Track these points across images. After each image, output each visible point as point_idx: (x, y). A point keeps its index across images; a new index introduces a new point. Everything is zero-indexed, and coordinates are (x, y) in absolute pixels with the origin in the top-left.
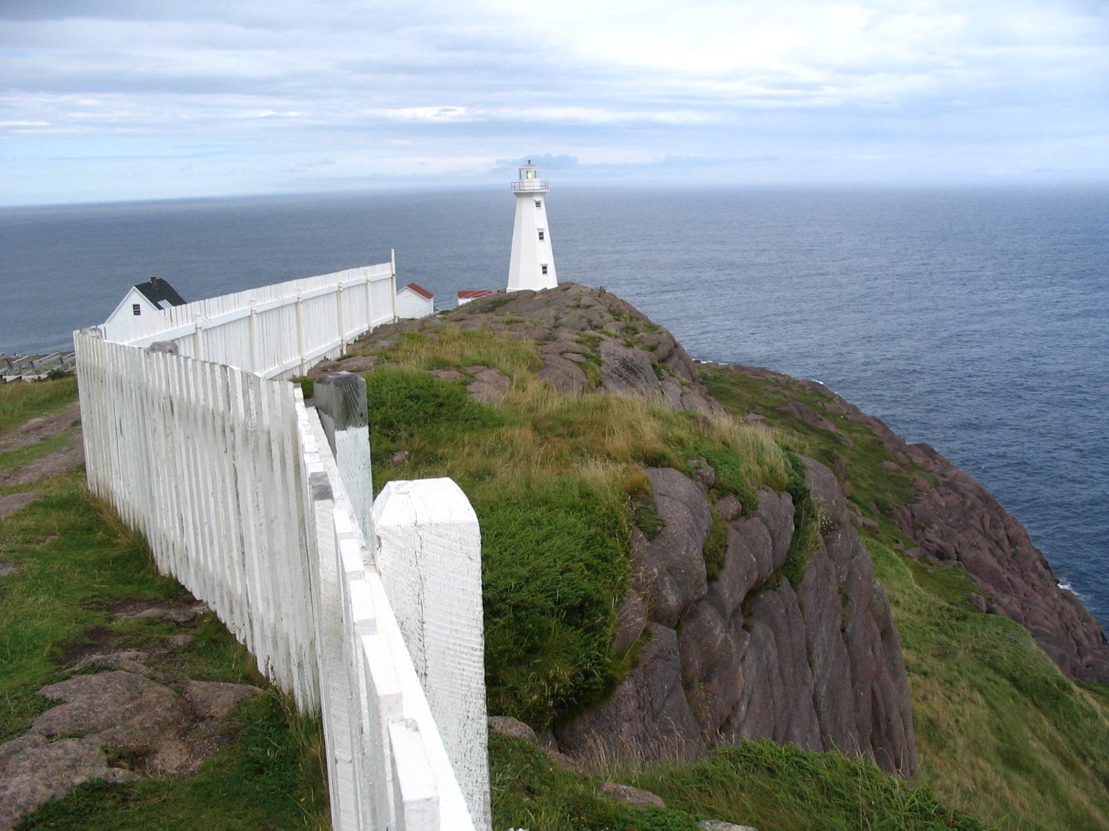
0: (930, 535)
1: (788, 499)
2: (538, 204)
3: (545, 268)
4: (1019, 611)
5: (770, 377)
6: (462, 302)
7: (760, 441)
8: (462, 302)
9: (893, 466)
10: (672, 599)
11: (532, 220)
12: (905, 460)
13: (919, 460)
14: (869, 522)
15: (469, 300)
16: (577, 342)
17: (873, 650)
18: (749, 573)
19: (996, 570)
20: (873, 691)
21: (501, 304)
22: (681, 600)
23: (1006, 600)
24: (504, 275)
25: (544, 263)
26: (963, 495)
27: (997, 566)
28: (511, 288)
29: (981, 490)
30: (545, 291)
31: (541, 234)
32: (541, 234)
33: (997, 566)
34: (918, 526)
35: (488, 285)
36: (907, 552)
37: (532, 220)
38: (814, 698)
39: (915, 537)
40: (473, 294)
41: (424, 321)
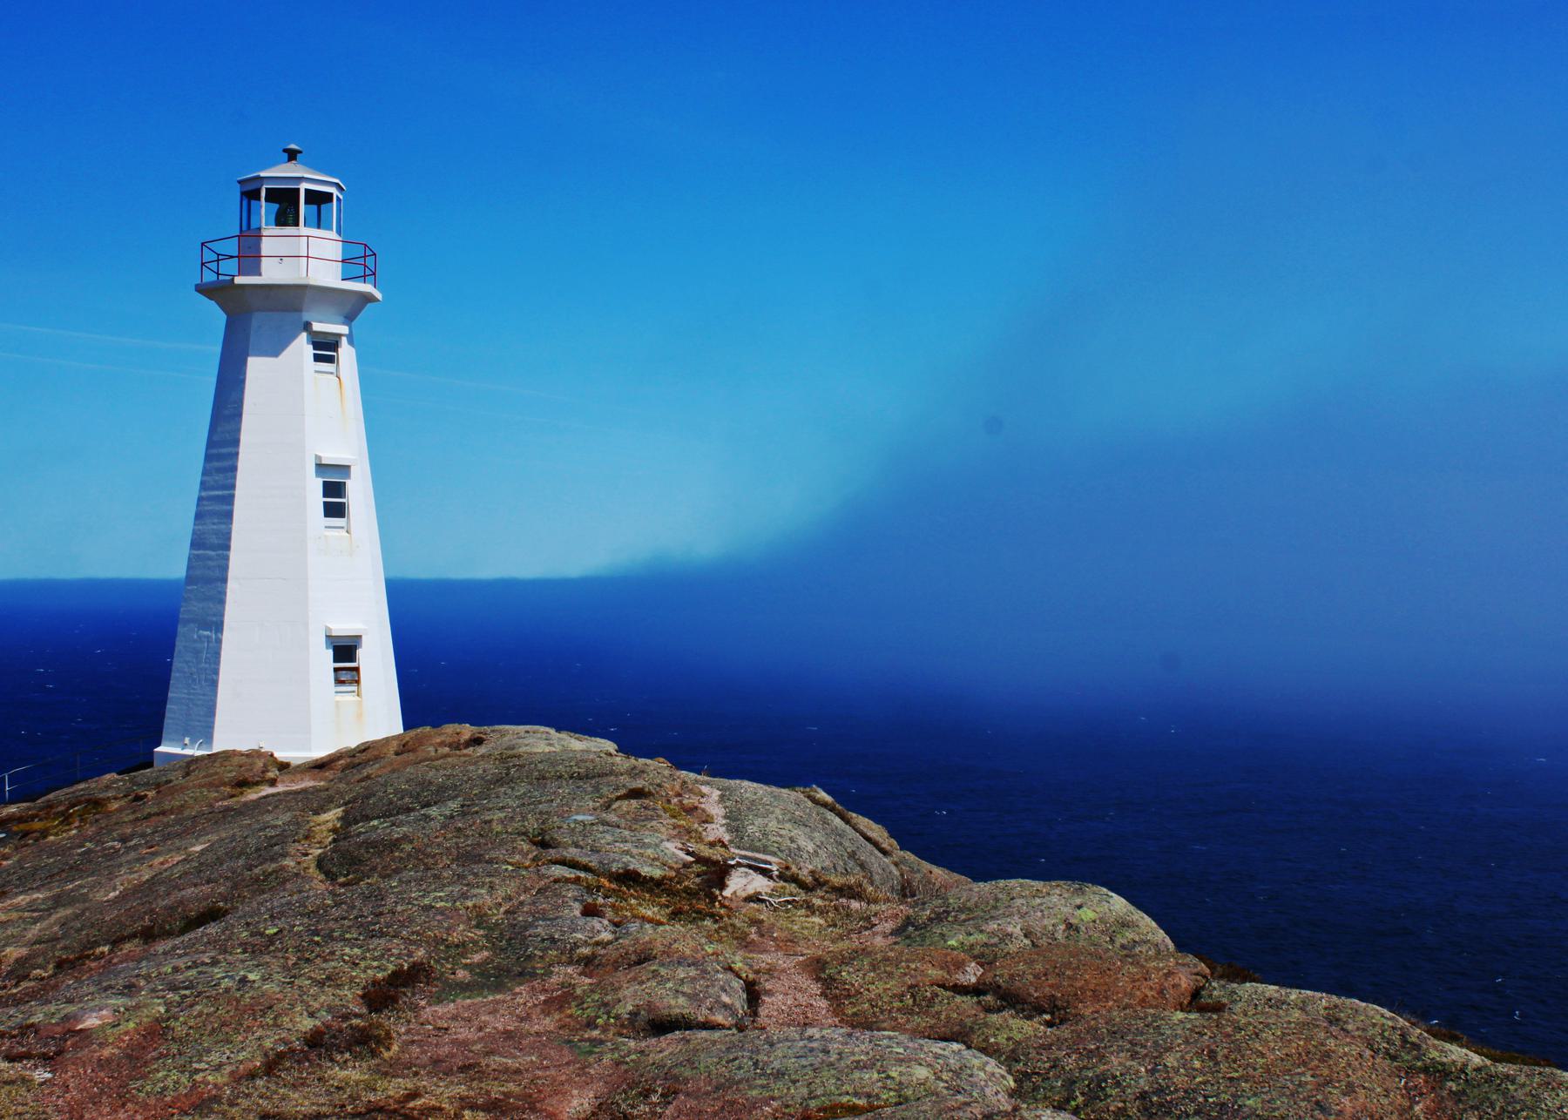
2: (325, 348)
3: (345, 651)
31: (334, 489)
32: (334, 489)
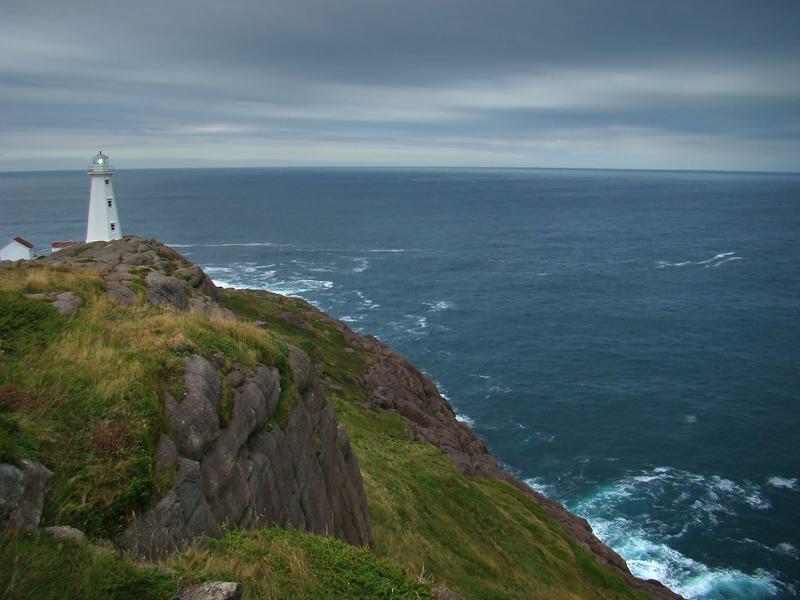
0: (376, 393)
1: (276, 372)
2: (107, 182)
4: (434, 438)
5: (269, 296)
6: (54, 250)
7: (293, 348)
8: (54, 250)
9: (351, 350)
10: (196, 441)
11: (99, 195)
12: (359, 347)
13: (367, 346)
14: (337, 387)
15: (59, 249)
16: (129, 272)
17: (340, 468)
18: (250, 420)
19: (420, 414)
20: (342, 496)
21: (83, 252)
22: (202, 441)
23: (426, 431)
24: (84, 231)
25: (113, 222)
26: (395, 366)
27: (420, 411)
28: (89, 240)
29: (406, 363)
30: (113, 242)
33: (420, 411)
34: (366, 388)
35: (75, 239)
36: (362, 405)
37: (99, 195)
38: (300, 502)
39: (367, 396)
40: (63, 245)
41: (776, 475)
